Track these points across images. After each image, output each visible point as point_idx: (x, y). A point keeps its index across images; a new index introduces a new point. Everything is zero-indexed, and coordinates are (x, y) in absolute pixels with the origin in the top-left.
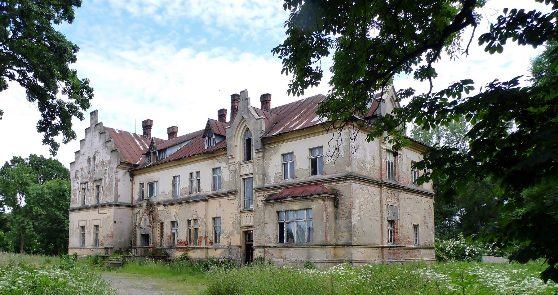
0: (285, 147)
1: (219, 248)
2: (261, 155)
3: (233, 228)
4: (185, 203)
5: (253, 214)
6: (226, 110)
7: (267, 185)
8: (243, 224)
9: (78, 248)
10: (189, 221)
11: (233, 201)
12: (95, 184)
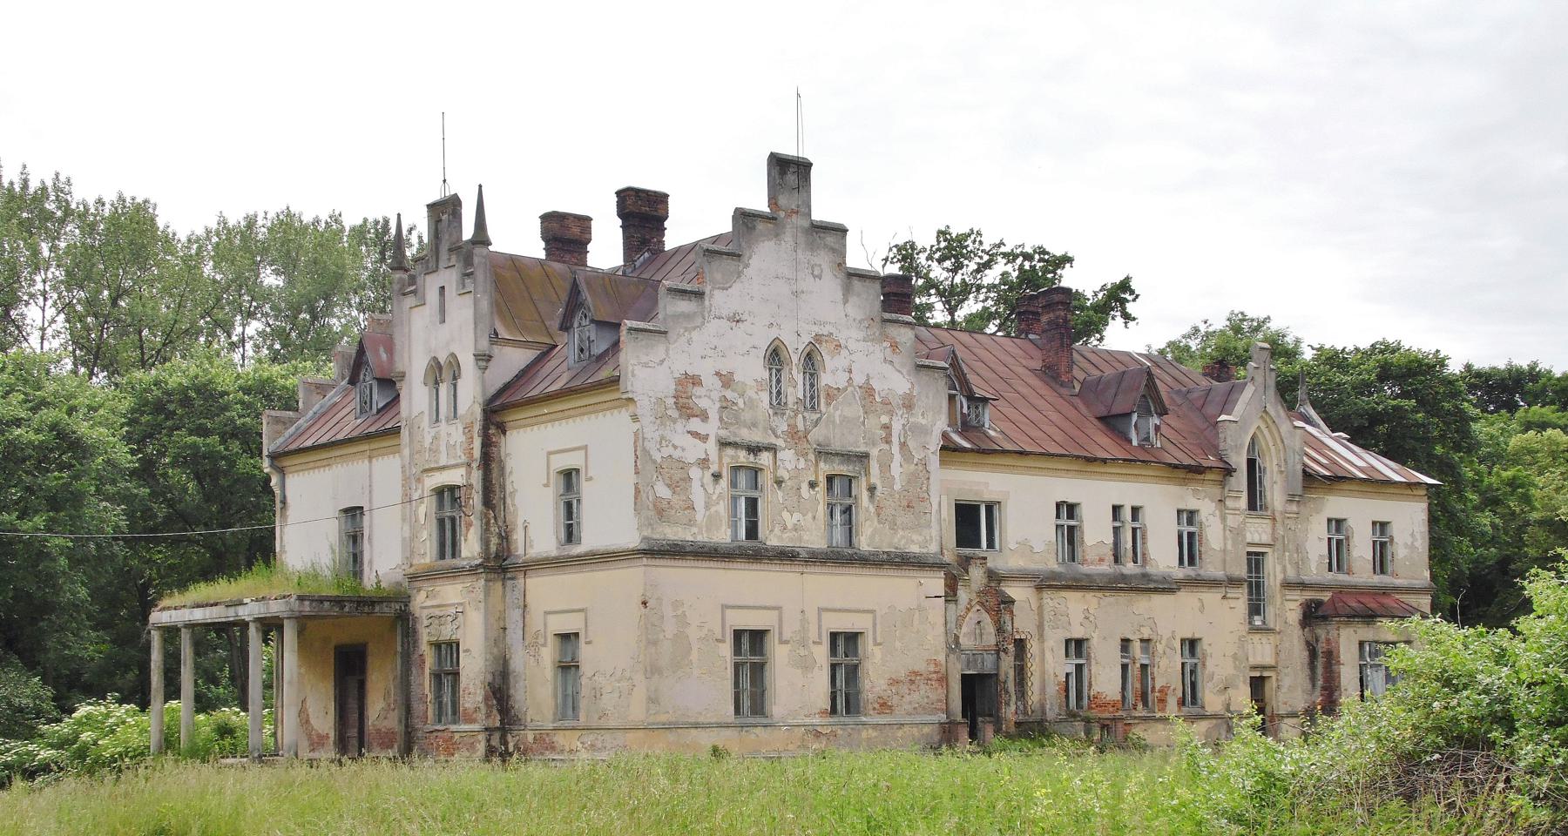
0: (1336, 504)
1: (1204, 717)
2: (1294, 508)
3: (1235, 667)
4: (1121, 589)
5: (1272, 637)
6: (584, 222)
7: (1306, 579)
8: (1252, 661)
9: (720, 726)
10: (1125, 643)
11: (1233, 603)
12: (825, 468)
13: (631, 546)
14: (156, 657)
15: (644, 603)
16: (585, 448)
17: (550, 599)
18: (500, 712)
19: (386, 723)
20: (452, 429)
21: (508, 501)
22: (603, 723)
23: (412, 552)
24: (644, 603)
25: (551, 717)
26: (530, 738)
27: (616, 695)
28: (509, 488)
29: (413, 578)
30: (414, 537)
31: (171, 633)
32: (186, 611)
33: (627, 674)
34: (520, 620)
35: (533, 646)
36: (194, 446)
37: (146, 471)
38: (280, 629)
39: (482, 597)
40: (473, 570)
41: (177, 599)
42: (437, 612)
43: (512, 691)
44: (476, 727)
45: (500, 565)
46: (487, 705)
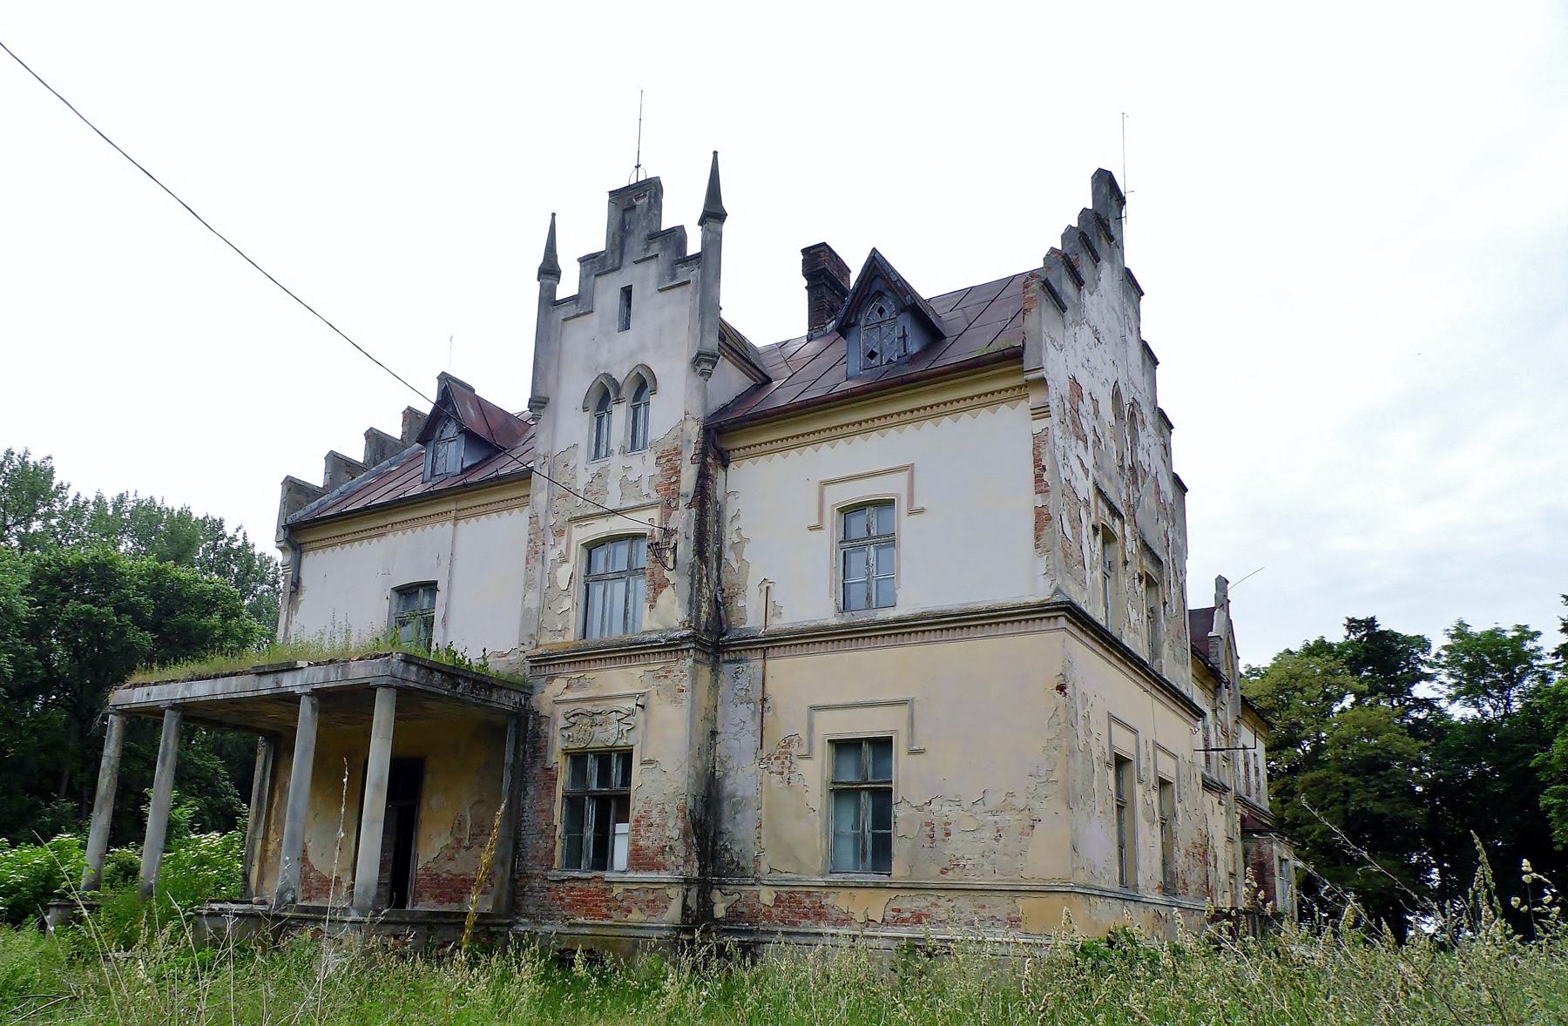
13: (1033, 600)
14: (111, 751)
15: (1061, 688)
16: (909, 468)
17: (817, 697)
18: (701, 855)
19: (450, 866)
20: (635, 461)
21: (729, 555)
22: (952, 878)
23: (540, 628)
24: (1061, 688)
25: (819, 867)
26: (767, 896)
27: (988, 834)
28: (730, 537)
29: (545, 662)
30: (546, 606)
31: (142, 723)
32: (181, 686)
33: (1020, 802)
34: (753, 726)
35: (780, 757)
36: (89, 613)
37: (35, 631)
38: (282, 744)
39: (686, 683)
40: (670, 647)
41: (157, 674)
42: (588, 707)
43: (727, 826)
44: (664, 876)
45: (716, 640)
46: (688, 846)
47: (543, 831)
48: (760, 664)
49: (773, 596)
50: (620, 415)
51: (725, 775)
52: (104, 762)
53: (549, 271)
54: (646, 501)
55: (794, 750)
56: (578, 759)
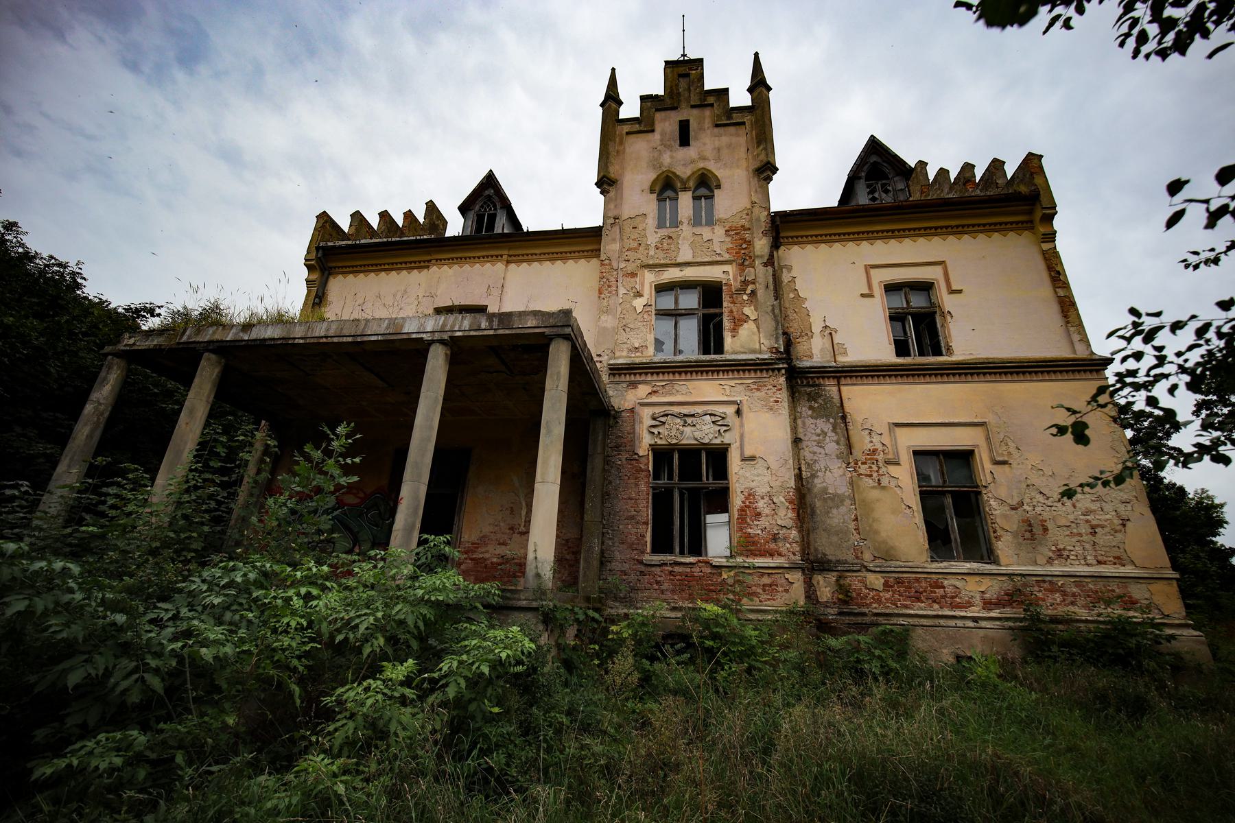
47: (633, 517)
48: (835, 389)
49: (837, 339)
50: (685, 201)
51: (813, 476)
52: (89, 408)
53: (612, 99)
54: (719, 259)
55: (881, 457)
56: (662, 455)
